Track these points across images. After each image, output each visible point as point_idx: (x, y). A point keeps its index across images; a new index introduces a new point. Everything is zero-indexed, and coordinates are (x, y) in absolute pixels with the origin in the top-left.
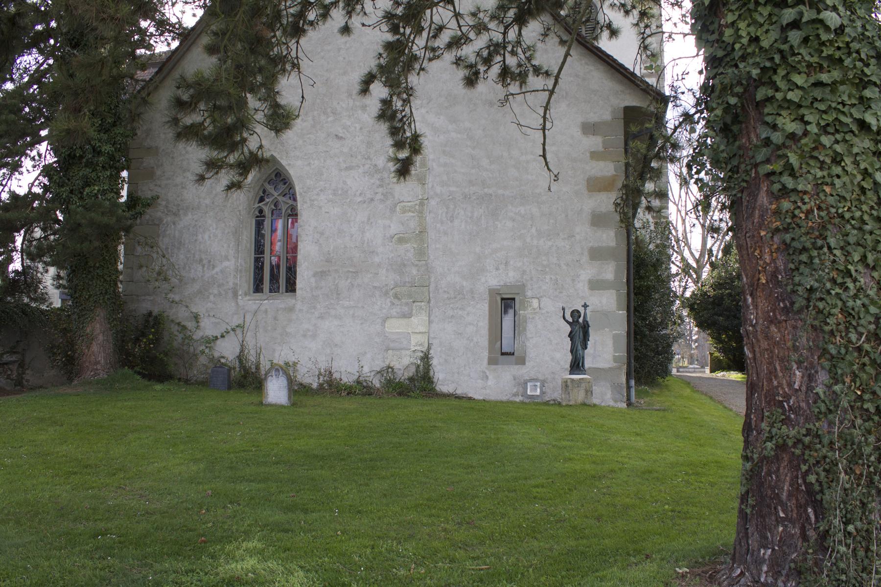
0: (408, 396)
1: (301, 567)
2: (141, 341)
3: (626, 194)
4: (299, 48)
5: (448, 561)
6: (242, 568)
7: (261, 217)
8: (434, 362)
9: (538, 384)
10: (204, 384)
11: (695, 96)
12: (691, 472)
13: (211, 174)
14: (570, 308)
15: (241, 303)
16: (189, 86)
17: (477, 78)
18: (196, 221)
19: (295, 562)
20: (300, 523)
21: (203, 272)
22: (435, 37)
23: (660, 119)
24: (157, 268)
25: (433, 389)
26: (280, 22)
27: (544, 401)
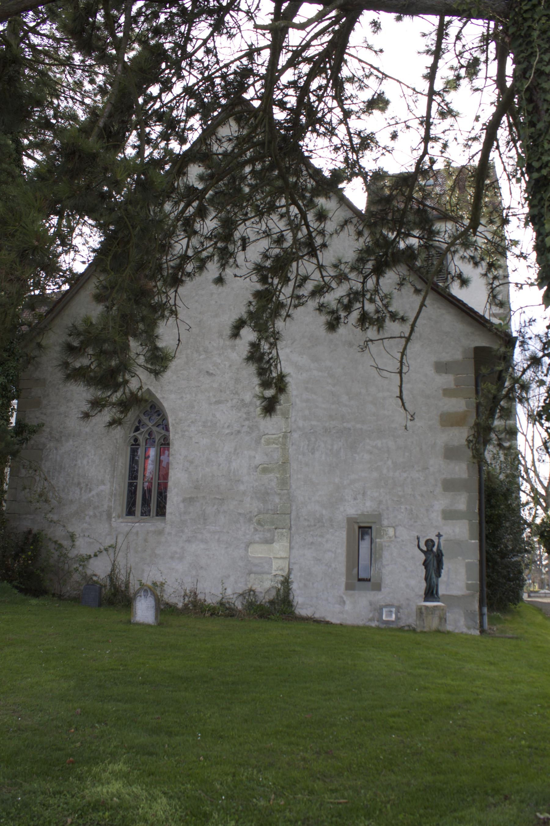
0: (269, 619)
1: (165, 793)
2: (20, 557)
3: (479, 433)
4: (177, 298)
5: (306, 793)
6: (108, 792)
7: (136, 445)
8: (294, 586)
9: (394, 610)
10: (76, 600)
11: (541, 341)
12: (546, 705)
13: (95, 412)
14: (424, 537)
15: (114, 524)
16: (79, 334)
17: (338, 323)
18: (77, 447)
19: (158, 788)
20: (164, 746)
21: (81, 494)
22: (300, 286)
23: (508, 358)
24: (39, 489)
25: (292, 613)
26: (161, 274)
27: (399, 627)
